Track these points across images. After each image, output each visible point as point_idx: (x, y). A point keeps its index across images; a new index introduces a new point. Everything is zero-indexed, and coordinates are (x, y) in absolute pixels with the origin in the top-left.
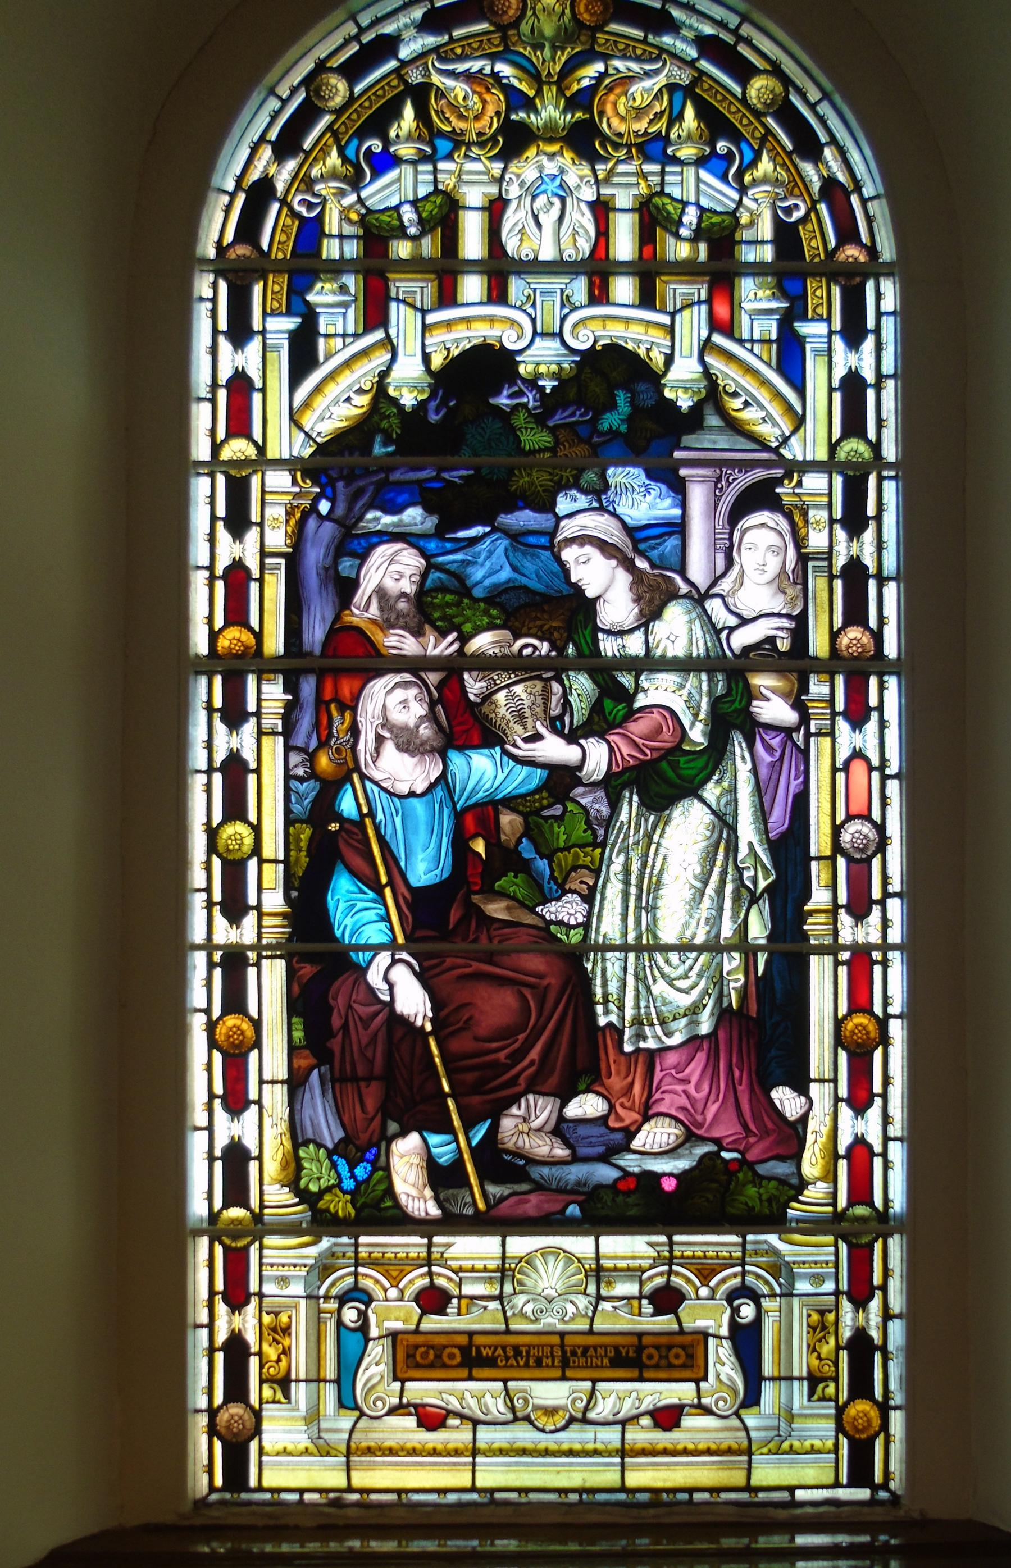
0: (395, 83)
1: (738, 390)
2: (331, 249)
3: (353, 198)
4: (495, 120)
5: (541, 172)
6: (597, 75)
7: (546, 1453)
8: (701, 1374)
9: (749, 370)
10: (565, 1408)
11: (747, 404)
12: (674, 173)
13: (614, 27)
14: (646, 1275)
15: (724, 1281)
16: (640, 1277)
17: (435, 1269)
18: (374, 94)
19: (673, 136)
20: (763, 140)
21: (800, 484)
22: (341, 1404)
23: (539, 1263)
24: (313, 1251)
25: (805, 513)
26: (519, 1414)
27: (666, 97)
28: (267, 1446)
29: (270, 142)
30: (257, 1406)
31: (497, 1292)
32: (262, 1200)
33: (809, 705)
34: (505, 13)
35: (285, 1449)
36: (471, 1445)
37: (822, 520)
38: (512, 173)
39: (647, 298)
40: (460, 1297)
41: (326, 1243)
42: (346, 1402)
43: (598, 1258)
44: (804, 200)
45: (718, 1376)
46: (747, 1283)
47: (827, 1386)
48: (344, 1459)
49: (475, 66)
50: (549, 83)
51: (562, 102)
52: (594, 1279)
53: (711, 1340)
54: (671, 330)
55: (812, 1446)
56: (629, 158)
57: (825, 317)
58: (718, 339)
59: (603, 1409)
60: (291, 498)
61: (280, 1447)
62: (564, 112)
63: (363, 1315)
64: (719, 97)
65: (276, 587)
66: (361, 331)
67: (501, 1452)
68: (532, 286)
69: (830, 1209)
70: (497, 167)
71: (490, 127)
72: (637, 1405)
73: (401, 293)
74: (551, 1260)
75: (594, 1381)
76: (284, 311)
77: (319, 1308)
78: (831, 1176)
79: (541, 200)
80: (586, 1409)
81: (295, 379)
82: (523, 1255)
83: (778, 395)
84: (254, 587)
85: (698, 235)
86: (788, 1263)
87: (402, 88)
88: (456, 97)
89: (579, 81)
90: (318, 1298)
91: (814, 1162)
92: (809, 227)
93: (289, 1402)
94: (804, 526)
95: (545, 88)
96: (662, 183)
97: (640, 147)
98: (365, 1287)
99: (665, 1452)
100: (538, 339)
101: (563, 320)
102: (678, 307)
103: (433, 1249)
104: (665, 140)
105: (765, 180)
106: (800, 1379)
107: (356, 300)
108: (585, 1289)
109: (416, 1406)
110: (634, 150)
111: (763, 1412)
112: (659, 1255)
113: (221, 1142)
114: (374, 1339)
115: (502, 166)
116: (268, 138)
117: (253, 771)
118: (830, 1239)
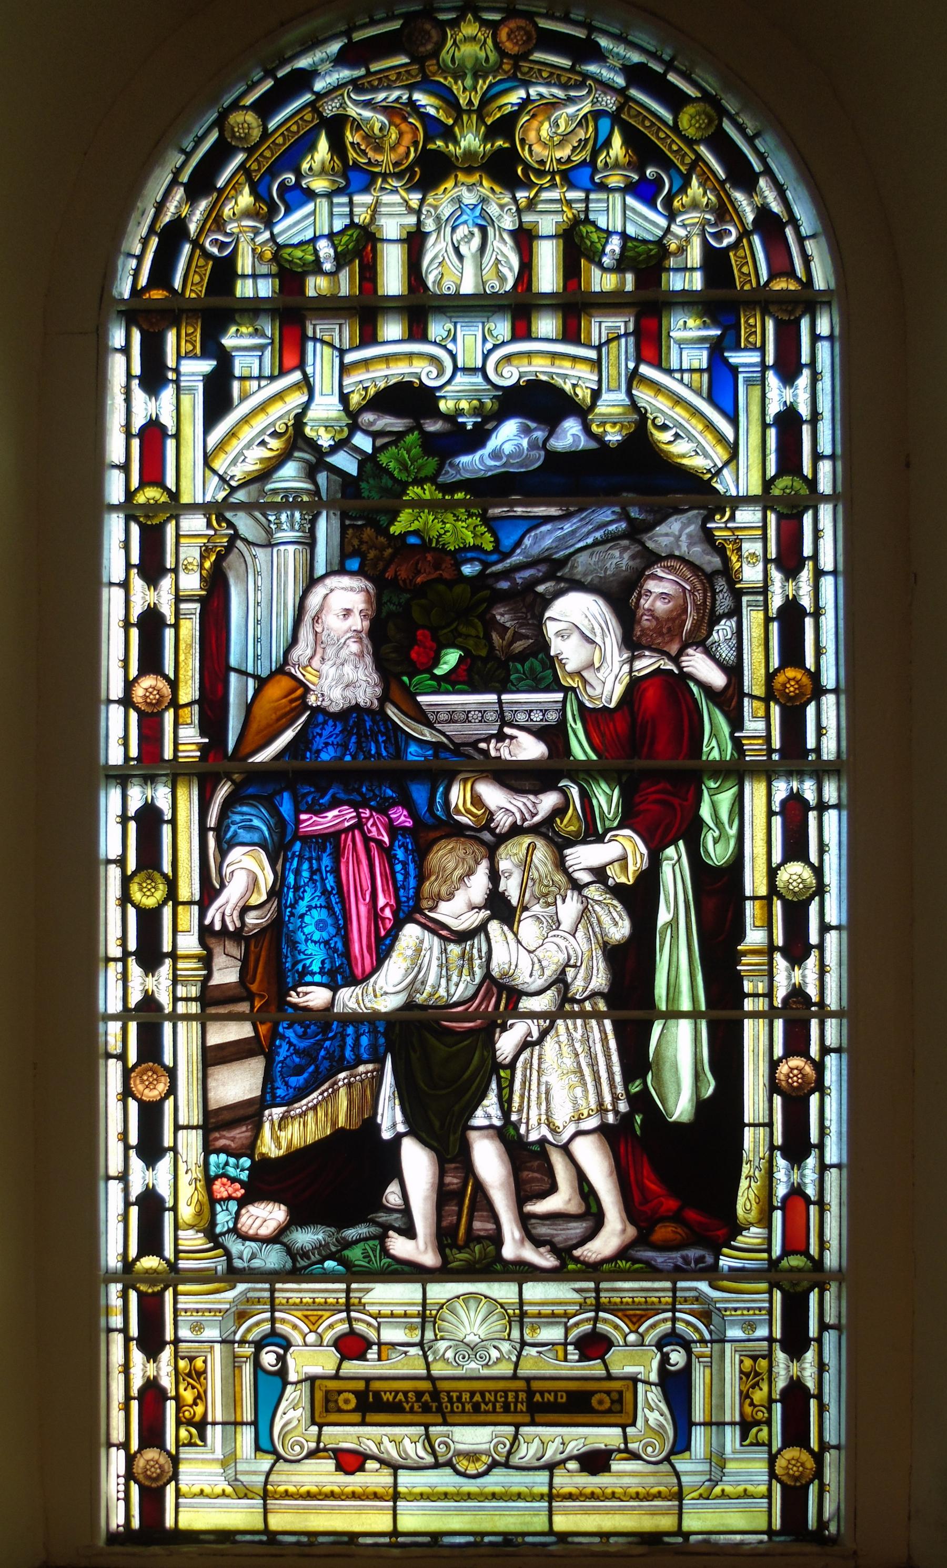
0: (308, 117)
1: (667, 422)
2: (244, 289)
3: (267, 235)
4: (412, 149)
6: (519, 101)
7: (469, 1496)
8: (630, 1421)
9: (678, 400)
10: (488, 1453)
11: (677, 436)
12: (598, 201)
13: (538, 56)
14: (572, 1321)
15: (653, 1326)
16: (566, 1323)
17: (353, 1314)
18: (288, 129)
19: (600, 164)
20: (693, 167)
21: (732, 518)
22: (258, 1448)
25: (738, 542)
26: (441, 1460)
27: (591, 124)
28: (184, 1488)
29: (182, 183)
30: (173, 1452)
31: (417, 1339)
32: (176, 1244)
35: (202, 1491)
36: (391, 1490)
38: (430, 205)
39: (571, 334)
40: (380, 1344)
41: (241, 1287)
45: (647, 1421)
47: (761, 1430)
50: (469, 112)
51: (483, 129)
52: (518, 1324)
53: (640, 1385)
56: (554, 186)
57: (758, 345)
58: (644, 369)
59: (527, 1452)
60: (206, 541)
61: (196, 1489)
63: (281, 1359)
64: (647, 124)
65: (190, 629)
66: (276, 373)
67: (422, 1496)
69: (765, 1255)
70: (414, 198)
72: (561, 1449)
73: (318, 331)
74: (472, 1304)
75: (517, 1426)
77: (234, 1352)
79: (462, 231)
81: (210, 422)
83: (710, 426)
84: (169, 634)
85: (620, 267)
86: (719, 1309)
88: (372, 128)
89: (500, 108)
90: (233, 1342)
91: (748, 1208)
92: (741, 253)
93: (205, 1446)
94: (738, 561)
95: (465, 118)
97: (565, 175)
98: (284, 1333)
99: (593, 1496)
100: (459, 374)
101: (485, 357)
102: (603, 341)
103: (352, 1295)
106: (732, 1424)
107: (272, 343)
108: (509, 1335)
109: (334, 1450)
110: (558, 178)
111: (693, 1457)
113: (136, 1190)
114: (292, 1383)
115: (420, 196)
116: (180, 180)
117: (168, 822)
118: (764, 1286)
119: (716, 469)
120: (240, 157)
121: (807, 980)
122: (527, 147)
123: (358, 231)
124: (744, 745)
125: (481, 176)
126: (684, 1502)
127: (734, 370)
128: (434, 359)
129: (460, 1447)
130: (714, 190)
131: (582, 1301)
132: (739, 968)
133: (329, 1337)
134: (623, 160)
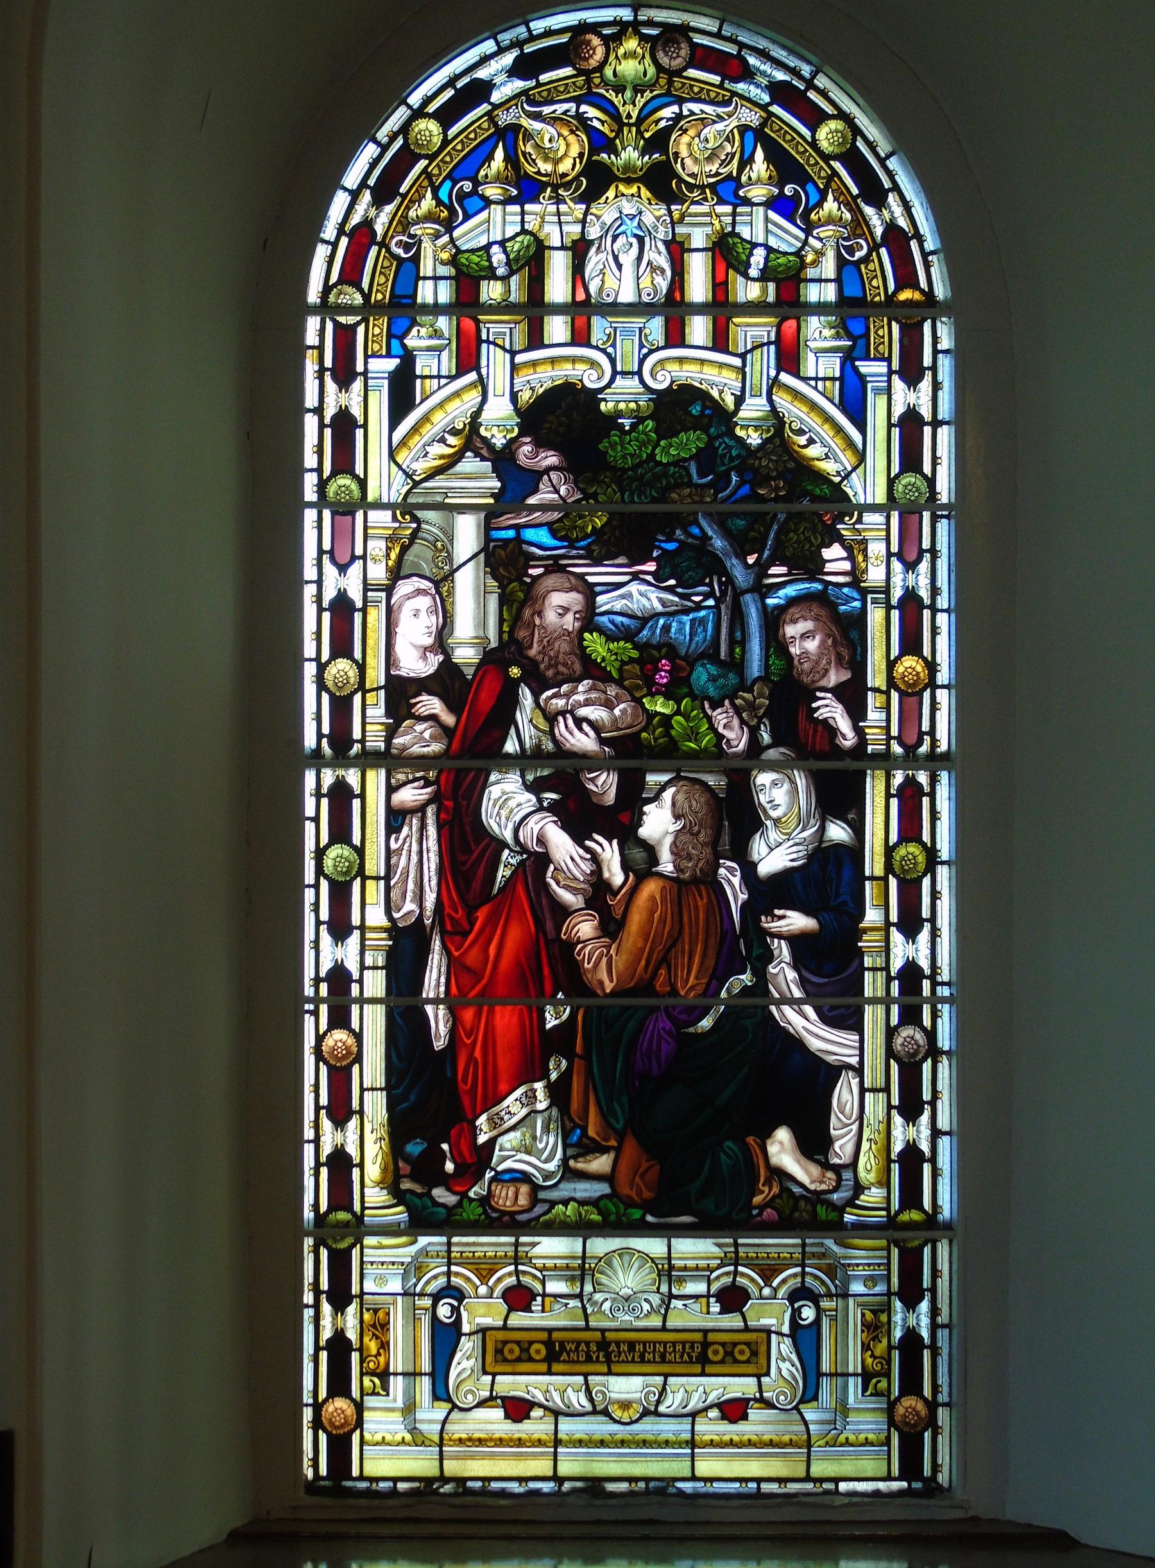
3: (446, 238)
5: (621, 212)
6: (674, 116)
8: (764, 1371)
9: (813, 406)
11: (811, 442)
15: (784, 1281)
16: (709, 1277)
19: (744, 179)
21: (860, 520)
22: (436, 1397)
23: (616, 1262)
24: (413, 1249)
25: (864, 542)
26: (598, 1408)
28: (367, 1436)
30: (358, 1399)
33: (867, 731)
34: (586, 59)
37: (881, 555)
39: (720, 341)
40: (544, 1295)
41: (423, 1241)
42: (441, 1393)
43: (669, 1258)
44: (866, 240)
45: (779, 1370)
46: (807, 1284)
47: (879, 1381)
48: (438, 1449)
49: (560, 108)
50: (630, 125)
53: (773, 1336)
54: (742, 371)
55: (866, 1439)
57: (886, 355)
58: (785, 377)
59: (672, 1403)
61: (378, 1438)
62: (643, 155)
63: (455, 1310)
66: (454, 372)
67: (580, 1443)
68: (613, 325)
69: (884, 1213)
71: (573, 169)
74: (626, 1258)
75: (666, 1376)
76: (384, 353)
78: (885, 1183)
79: (621, 240)
80: (658, 1402)
81: (395, 418)
82: (602, 1255)
83: (839, 430)
85: (765, 276)
86: (843, 1265)
87: (492, 130)
89: (657, 122)
90: (414, 1295)
91: (869, 1167)
92: (871, 266)
93: (388, 1395)
95: (626, 130)
96: (734, 224)
97: (714, 192)
102: (749, 347)
104: (734, 181)
105: (830, 220)
106: (855, 1375)
108: (658, 1288)
110: (708, 191)
111: (820, 1406)
112: (726, 1256)
114: (466, 1335)
118: (884, 1243)
119: (846, 472)
120: (423, 163)
121: (902, 1129)
122: (679, 160)
123: (528, 237)
124: (867, 734)
125: (639, 188)
126: (812, 1449)
127: (862, 379)
128: (593, 364)
129: (614, 1396)
130: (847, 205)
131: (723, 1255)
132: (860, 944)
133: (498, 1291)
134: (765, 175)
